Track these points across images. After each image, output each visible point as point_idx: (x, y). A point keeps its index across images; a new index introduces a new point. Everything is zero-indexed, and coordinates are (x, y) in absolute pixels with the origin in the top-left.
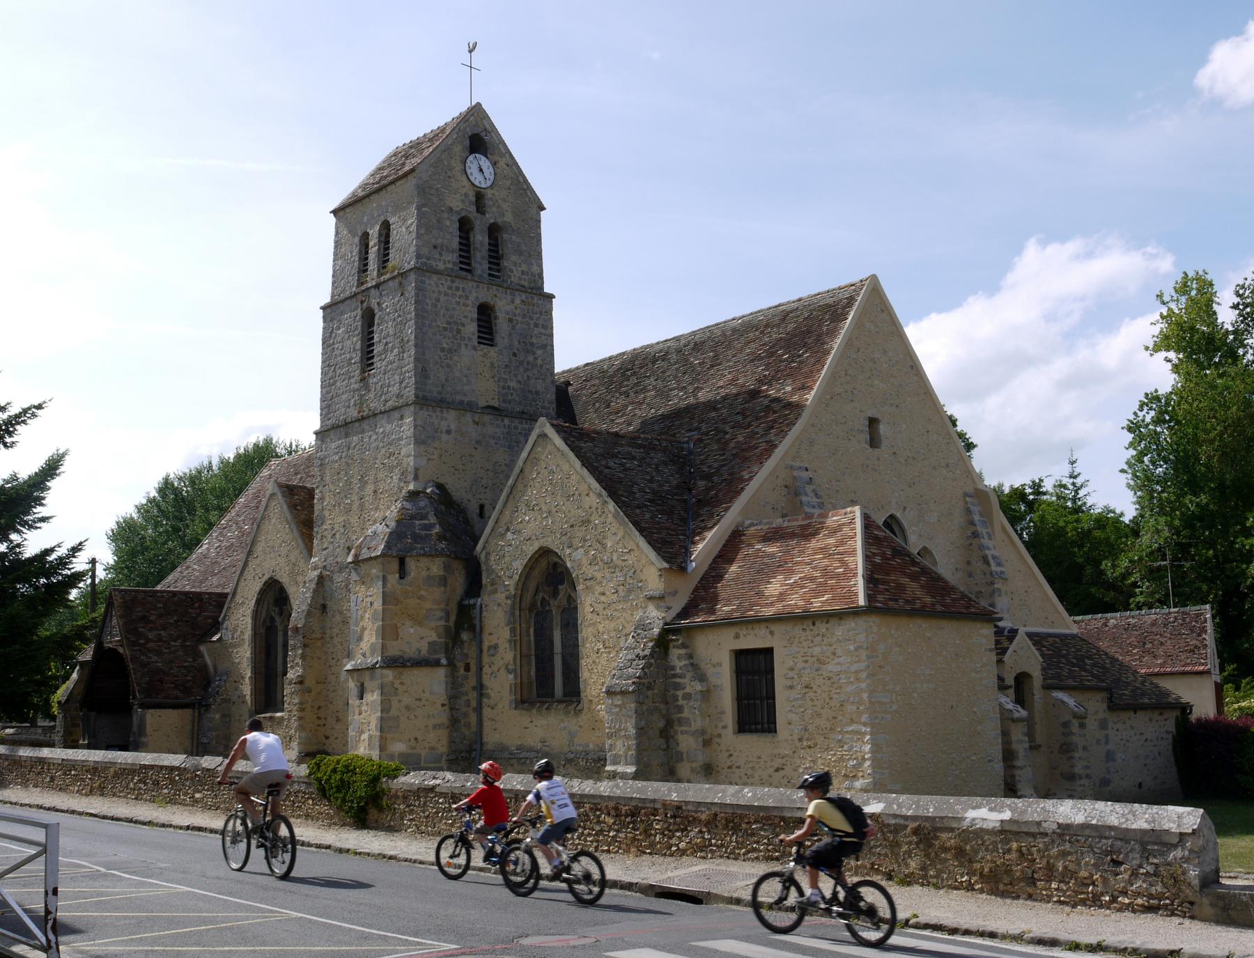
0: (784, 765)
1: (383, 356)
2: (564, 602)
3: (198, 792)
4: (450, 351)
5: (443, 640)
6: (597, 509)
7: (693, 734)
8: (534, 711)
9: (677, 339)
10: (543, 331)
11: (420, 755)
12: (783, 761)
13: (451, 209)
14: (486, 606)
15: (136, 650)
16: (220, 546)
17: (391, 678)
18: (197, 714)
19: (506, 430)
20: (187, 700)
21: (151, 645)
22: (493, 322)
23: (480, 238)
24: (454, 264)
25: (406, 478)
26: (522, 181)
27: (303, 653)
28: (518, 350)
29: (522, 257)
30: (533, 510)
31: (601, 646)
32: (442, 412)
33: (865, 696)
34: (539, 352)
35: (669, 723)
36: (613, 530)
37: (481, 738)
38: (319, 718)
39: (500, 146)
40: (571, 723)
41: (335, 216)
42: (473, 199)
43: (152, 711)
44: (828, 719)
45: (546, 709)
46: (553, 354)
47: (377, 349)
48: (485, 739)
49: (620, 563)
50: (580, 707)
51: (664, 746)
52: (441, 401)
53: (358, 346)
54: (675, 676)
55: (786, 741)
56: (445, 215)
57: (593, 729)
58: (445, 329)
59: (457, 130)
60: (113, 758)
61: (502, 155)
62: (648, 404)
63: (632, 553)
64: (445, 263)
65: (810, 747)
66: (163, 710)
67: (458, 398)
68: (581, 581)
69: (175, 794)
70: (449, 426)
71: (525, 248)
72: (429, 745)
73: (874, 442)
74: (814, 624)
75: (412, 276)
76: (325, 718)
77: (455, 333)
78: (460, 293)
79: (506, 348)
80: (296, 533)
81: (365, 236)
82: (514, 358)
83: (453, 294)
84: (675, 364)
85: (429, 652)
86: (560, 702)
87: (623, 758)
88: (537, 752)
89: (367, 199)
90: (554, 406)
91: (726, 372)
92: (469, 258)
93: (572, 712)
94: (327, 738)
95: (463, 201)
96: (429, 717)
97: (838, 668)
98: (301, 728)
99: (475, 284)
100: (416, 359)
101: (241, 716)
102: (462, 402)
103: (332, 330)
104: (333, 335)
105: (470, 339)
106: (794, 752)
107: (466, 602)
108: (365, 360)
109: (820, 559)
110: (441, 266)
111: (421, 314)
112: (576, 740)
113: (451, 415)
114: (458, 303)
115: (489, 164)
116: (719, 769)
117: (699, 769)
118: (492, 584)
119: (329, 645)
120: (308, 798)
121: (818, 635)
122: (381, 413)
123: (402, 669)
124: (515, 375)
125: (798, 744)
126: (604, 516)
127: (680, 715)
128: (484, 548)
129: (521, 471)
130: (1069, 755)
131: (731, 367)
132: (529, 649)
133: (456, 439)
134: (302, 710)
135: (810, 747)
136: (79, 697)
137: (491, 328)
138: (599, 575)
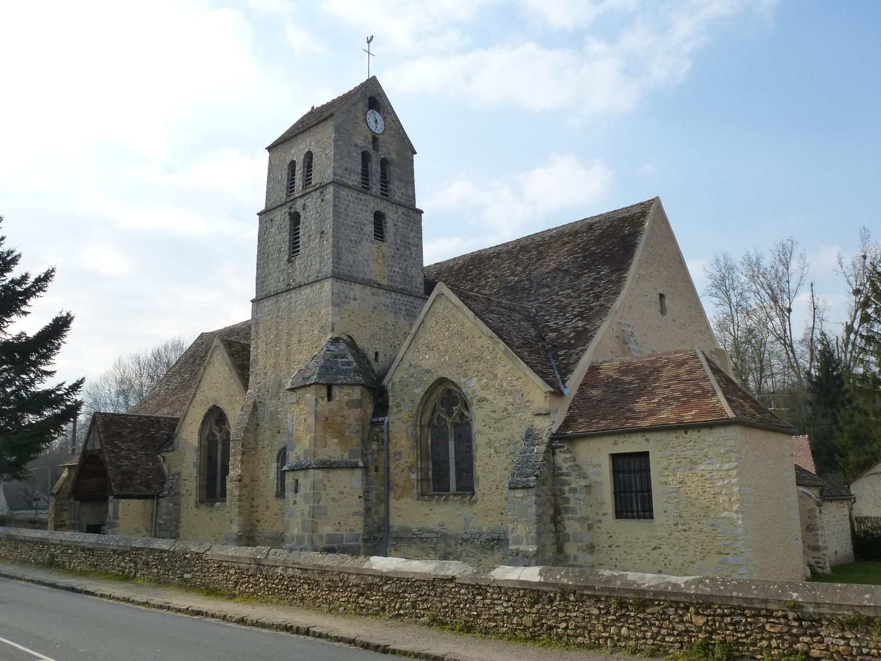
0: (661, 545)
1: (307, 245)
3: (187, 573)
4: (356, 242)
6: (488, 348)
7: (579, 520)
8: (434, 502)
9: (506, 244)
10: (416, 235)
11: (343, 536)
12: (660, 542)
13: (356, 145)
16: (167, 388)
17: (321, 476)
18: (155, 503)
19: (393, 301)
20: (149, 493)
23: (375, 167)
24: (358, 182)
25: (325, 330)
26: (402, 132)
27: (241, 459)
28: (400, 246)
29: (402, 184)
30: (433, 350)
31: (493, 452)
32: (351, 285)
33: (736, 489)
34: (414, 249)
35: (557, 511)
36: (503, 363)
37: (388, 523)
40: (467, 511)
41: (269, 152)
42: (371, 140)
43: (123, 501)
44: (702, 508)
46: (422, 251)
48: (391, 523)
49: (509, 388)
50: (474, 498)
51: (553, 530)
52: (350, 276)
53: (287, 238)
54: (562, 474)
55: (662, 525)
56: (353, 149)
57: (486, 516)
58: (353, 227)
61: (389, 114)
62: (490, 286)
63: (520, 380)
65: (685, 530)
67: (361, 276)
68: (475, 402)
69: (164, 574)
70: (355, 295)
71: (403, 178)
72: (350, 528)
73: (663, 311)
74: (686, 433)
75: (331, 189)
76: (257, 507)
77: (359, 230)
78: (363, 202)
79: (392, 244)
80: (234, 374)
81: (293, 164)
84: (507, 260)
85: (350, 457)
86: (455, 495)
87: (524, 539)
90: (423, 287)
91: (551, 263)
92: (367, 180)
93: (467, 503)
94: (258, 521)
95: (364, 141)
97: (710, 468)
98: (240, 514)
99: (372, 198)
100: (334, 246)
102: (363, 279)
103: (267, 229)
104: (267, 232)
105: (369, 235)
106: (670, 534)
107: (376, 420)
109: (675, 384)
110: (350, 183)
111: (337, 213)
112: (470, 524)
113: (357, 287)
114: (361, 210)
115: (381, 118)
117: (585, 548)
119: (260, 453)
121: (691, 441)
122: (305, 284)
124: (399, 264)
125: (674, 528)
126: (494, 353)
127: (567, 505)
128: (391, 379)
129: (423, 322)
130: (814, 533)
133: (360, 304)
134: (240, 500)
135: (685, 530)
137: (382, 229)
138: (490, 397)
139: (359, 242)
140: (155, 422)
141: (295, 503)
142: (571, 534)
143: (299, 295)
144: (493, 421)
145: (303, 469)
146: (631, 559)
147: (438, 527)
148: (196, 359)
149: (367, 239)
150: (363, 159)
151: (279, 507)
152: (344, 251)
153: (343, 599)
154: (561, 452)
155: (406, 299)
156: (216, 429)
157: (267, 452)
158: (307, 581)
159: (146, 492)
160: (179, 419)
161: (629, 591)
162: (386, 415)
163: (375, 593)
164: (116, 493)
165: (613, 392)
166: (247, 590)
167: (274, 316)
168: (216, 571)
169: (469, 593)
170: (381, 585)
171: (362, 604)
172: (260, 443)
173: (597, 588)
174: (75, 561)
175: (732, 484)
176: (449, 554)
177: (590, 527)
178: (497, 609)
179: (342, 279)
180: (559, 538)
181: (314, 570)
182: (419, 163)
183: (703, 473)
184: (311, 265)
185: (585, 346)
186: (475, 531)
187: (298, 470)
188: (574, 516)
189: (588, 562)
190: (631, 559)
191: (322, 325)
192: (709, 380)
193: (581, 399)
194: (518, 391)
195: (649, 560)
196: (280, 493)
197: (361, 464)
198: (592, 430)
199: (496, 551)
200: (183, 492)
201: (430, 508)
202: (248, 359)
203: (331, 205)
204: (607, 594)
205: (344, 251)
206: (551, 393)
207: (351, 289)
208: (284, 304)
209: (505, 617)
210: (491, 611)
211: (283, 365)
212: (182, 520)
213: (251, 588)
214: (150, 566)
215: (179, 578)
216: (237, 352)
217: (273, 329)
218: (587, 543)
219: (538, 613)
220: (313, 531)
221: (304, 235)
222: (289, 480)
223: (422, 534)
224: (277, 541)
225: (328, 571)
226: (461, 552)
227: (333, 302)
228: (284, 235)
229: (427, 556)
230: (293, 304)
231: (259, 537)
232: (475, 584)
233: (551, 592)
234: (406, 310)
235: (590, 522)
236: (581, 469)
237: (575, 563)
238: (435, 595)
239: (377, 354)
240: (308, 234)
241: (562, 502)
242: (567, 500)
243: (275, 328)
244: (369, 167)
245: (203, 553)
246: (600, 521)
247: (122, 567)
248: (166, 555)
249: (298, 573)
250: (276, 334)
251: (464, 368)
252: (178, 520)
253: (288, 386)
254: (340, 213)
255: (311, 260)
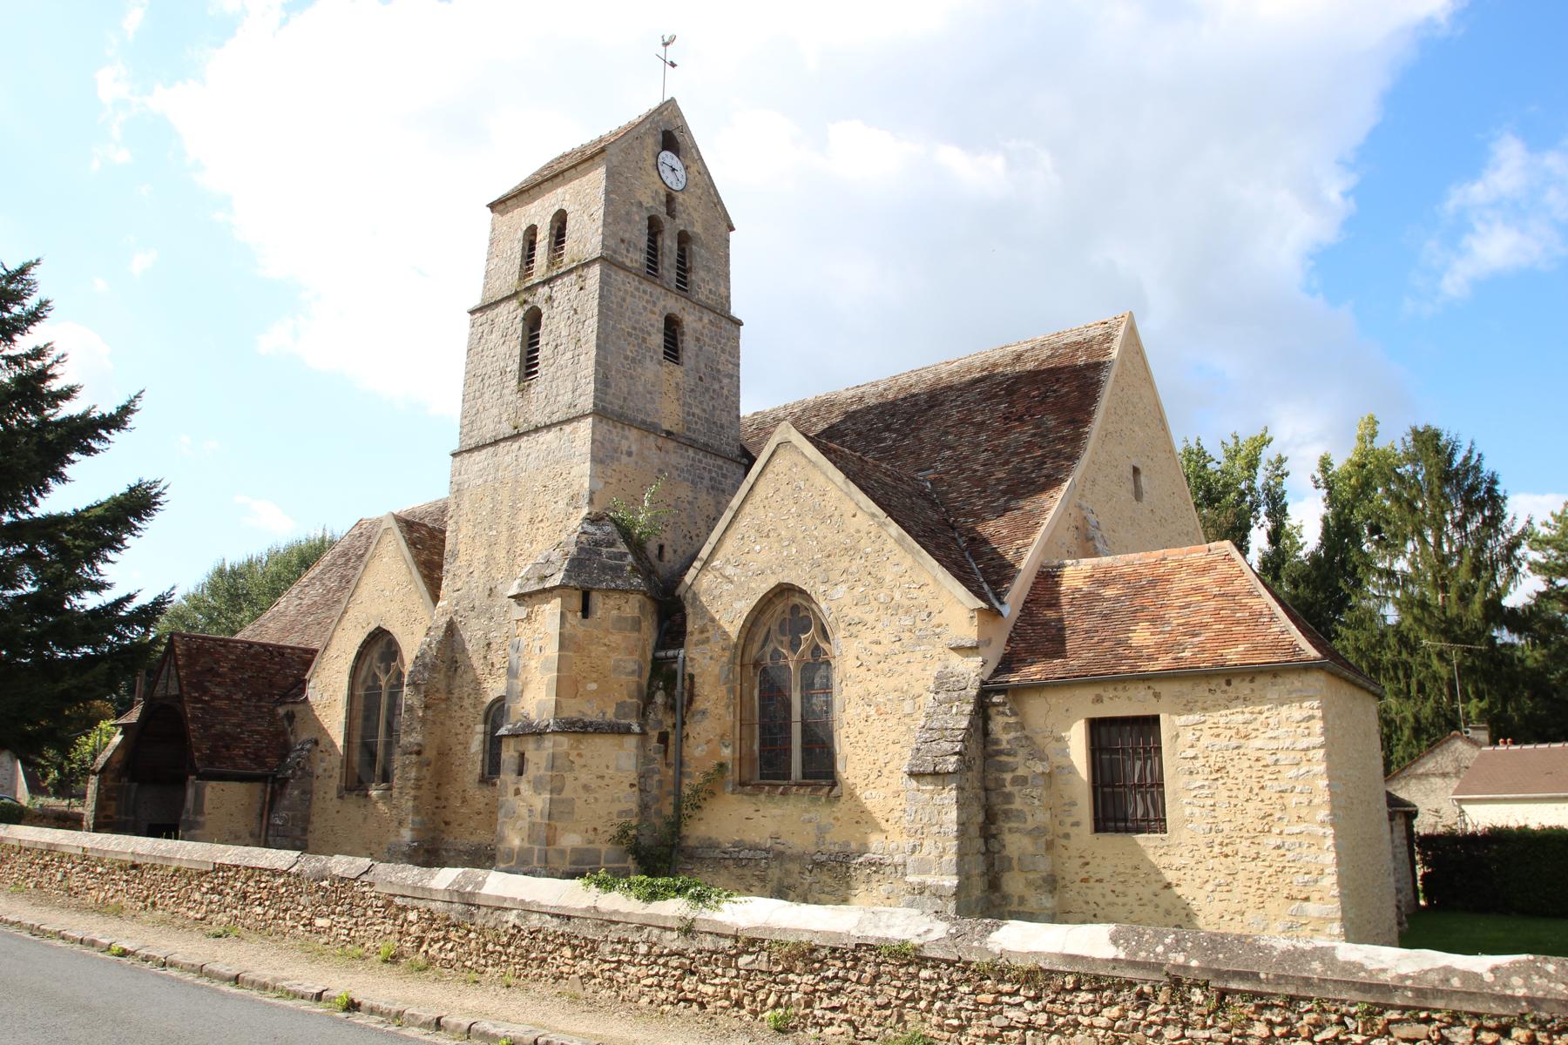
1: (552, 361)
2: (808, 657)
3: (322, 917)
4: (633, 360)
5: (634, 700)
7: (1029, 833)
8: (762, 797)
10: (730, 359)
11: (600, 852)
13: (640, 204)
14: (692, 659)
15: (199, 708)
17: (566, 747)
18: (269, 789)
19: (690, 462)
21: (217, 703)
22: (679, 337)
23: (669, 243)
25: (577, 502)
26: (712, 192)
30: (768, 536)
31: (873, 712)
34: (726, 381)
36: (895, 559)
38: (437, 798)
39: (693, 150)
40: (822, 814)
42: (664, 199)
45: (782, 794)
47: (544, 352)
49: (906, 602)
50: (835, 791)
51: (983, 849)
53: (517, 351)
56: (634, 209)
58: (630, 335)
59: (650, 120)
60: (168, 851)
63: (924, 588)
64: (631, 261)
66: (227, 783)
67: (641, 417)
68: (842, 625)
73: (1138, 495)
74: (1228, 683)
76: (447, 799)
78: (647, 297)
81: (532, 231)
82: (700, 383)
83: (640, 297)
85: (616, 715)
86: (800, 785)
88: (767, 851)
89: (537, 189)
91: (954, 412)
92: (655, 263)
93: (823, 799)
94: (447, 823)
95: (653, 198)
96: (613, 801)
97: (1274, 745)
98: (417, 810)
100: (598, 363)
101: (326, 793)
102: (644, 422)
104: (483, 341)
107: (662, 654)
108: (524, 369)
110: (628, 263)
112: (828, 837)
113: (633, 434)
116: (1066, 882)
117: (1040, 882)
118: (702, 632)
120: (563, 945)
123: (580, 736)
124: (701, 402)
127: (1006, 807)
131: (959, 406)
132: (752, 713)
133: (637, 463)
134: (418, 788)
135: (1227, 856)
136: (118, 766)
137: (676, 345)
138: (870, 618)
139: (639, 361)
140: (275, 653)
141: (517, 792)
142: (1015, 855)
143: (535, 443)
144: (874, 659)
145: (534, 734)
146: (1124, 905)
147: (769, 840)
148: (350, 559)
149: (652, 357)
150: (650, 227)
151: (486, 800)
152: (613, 373)
153: (649, 981)
154: (999, 713)
155: (711, 462)
156: (379, 668)
157: (468, 706)
158: (568, 940)
159: (254, 769)
160: (317, 651)
161: (1353, 985)
162: (681, 645)
163: (719, 971)
164: (201, 771)
165: (1086, 614)
166: (442, 956)
167: (490, 478)
168: (380, 915)
169: (940, 979)
170: (734, 956)
171: (691, 992)
172: (456, 691)
173: (1262, 976)
174: (107, 887)
175: (1315, 775)
176: (789, 888)
177: (1050, 846)
178: (1010, 1015)
179: (609, 418)
180: (993, 865)
181: (586, 919)
182: (739, 245)
183: (1259, 754)
184: (558, 395)
185: (1027, 537)
186: (837, 849)
187: (525, 735)
188: (1022, 826)
189: (1046, 908)
190: (1124, 905)
191: (572, 494)
192: (1259, 596)
193: (1029, 625)
194: (920, 609)
195: (1157, 906)
196: (486, 775)
197: (636, 728)
198: (1056, 676)
199: (874, 885)
200: (319, 771)
201: (754, 807)
202: (441, 554)
203: (597, 296)
204: (1291, 991)
205: (613, 373)
206: (980, 610)
207: (624, 437)
208: (508, 459)
209: (1029, 1033)
210: (995, 1020)
211: (502, 560)
212: (313, 819)
213: (451, 950)
214: (248, 901)
215: (304, 925)
216: (421, 540)
217: (488, 500)
218: (1045, 874)
219: (1112, 1028)
220: (550, 841)
221: (547, 344)
222: (508, 754)
223: (739, 852)
224: (483, 857)
225: (617, 923)
226: (811, 884)
227: (592, 456)
228: (512, 345)
229: (748, 890)
230: (522, 460)
231: (446, 850)
232: (957, 959)
233: (1146, 981)
234: (711, 479)
235: (1049, 837)
236: (1034, 743)
237: (1021, 909)
238: (858, 982)
239: (661, 547)
240: (554, 344)
241: (1000, 800)
242: (1008, 798)
243: (489, 498)
244: (660, 243)
245: (356, 880)
246: (1067, 836)
247: (195, 901)
248: (282, 880)
249: (552, 925)
250: (492, 509)
251: (824, 566)
252: (307, 820)
253: (514, 591)
254: (609, 309)
255: (557, 387)
